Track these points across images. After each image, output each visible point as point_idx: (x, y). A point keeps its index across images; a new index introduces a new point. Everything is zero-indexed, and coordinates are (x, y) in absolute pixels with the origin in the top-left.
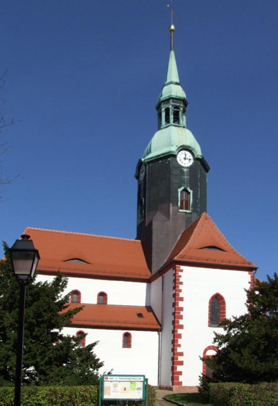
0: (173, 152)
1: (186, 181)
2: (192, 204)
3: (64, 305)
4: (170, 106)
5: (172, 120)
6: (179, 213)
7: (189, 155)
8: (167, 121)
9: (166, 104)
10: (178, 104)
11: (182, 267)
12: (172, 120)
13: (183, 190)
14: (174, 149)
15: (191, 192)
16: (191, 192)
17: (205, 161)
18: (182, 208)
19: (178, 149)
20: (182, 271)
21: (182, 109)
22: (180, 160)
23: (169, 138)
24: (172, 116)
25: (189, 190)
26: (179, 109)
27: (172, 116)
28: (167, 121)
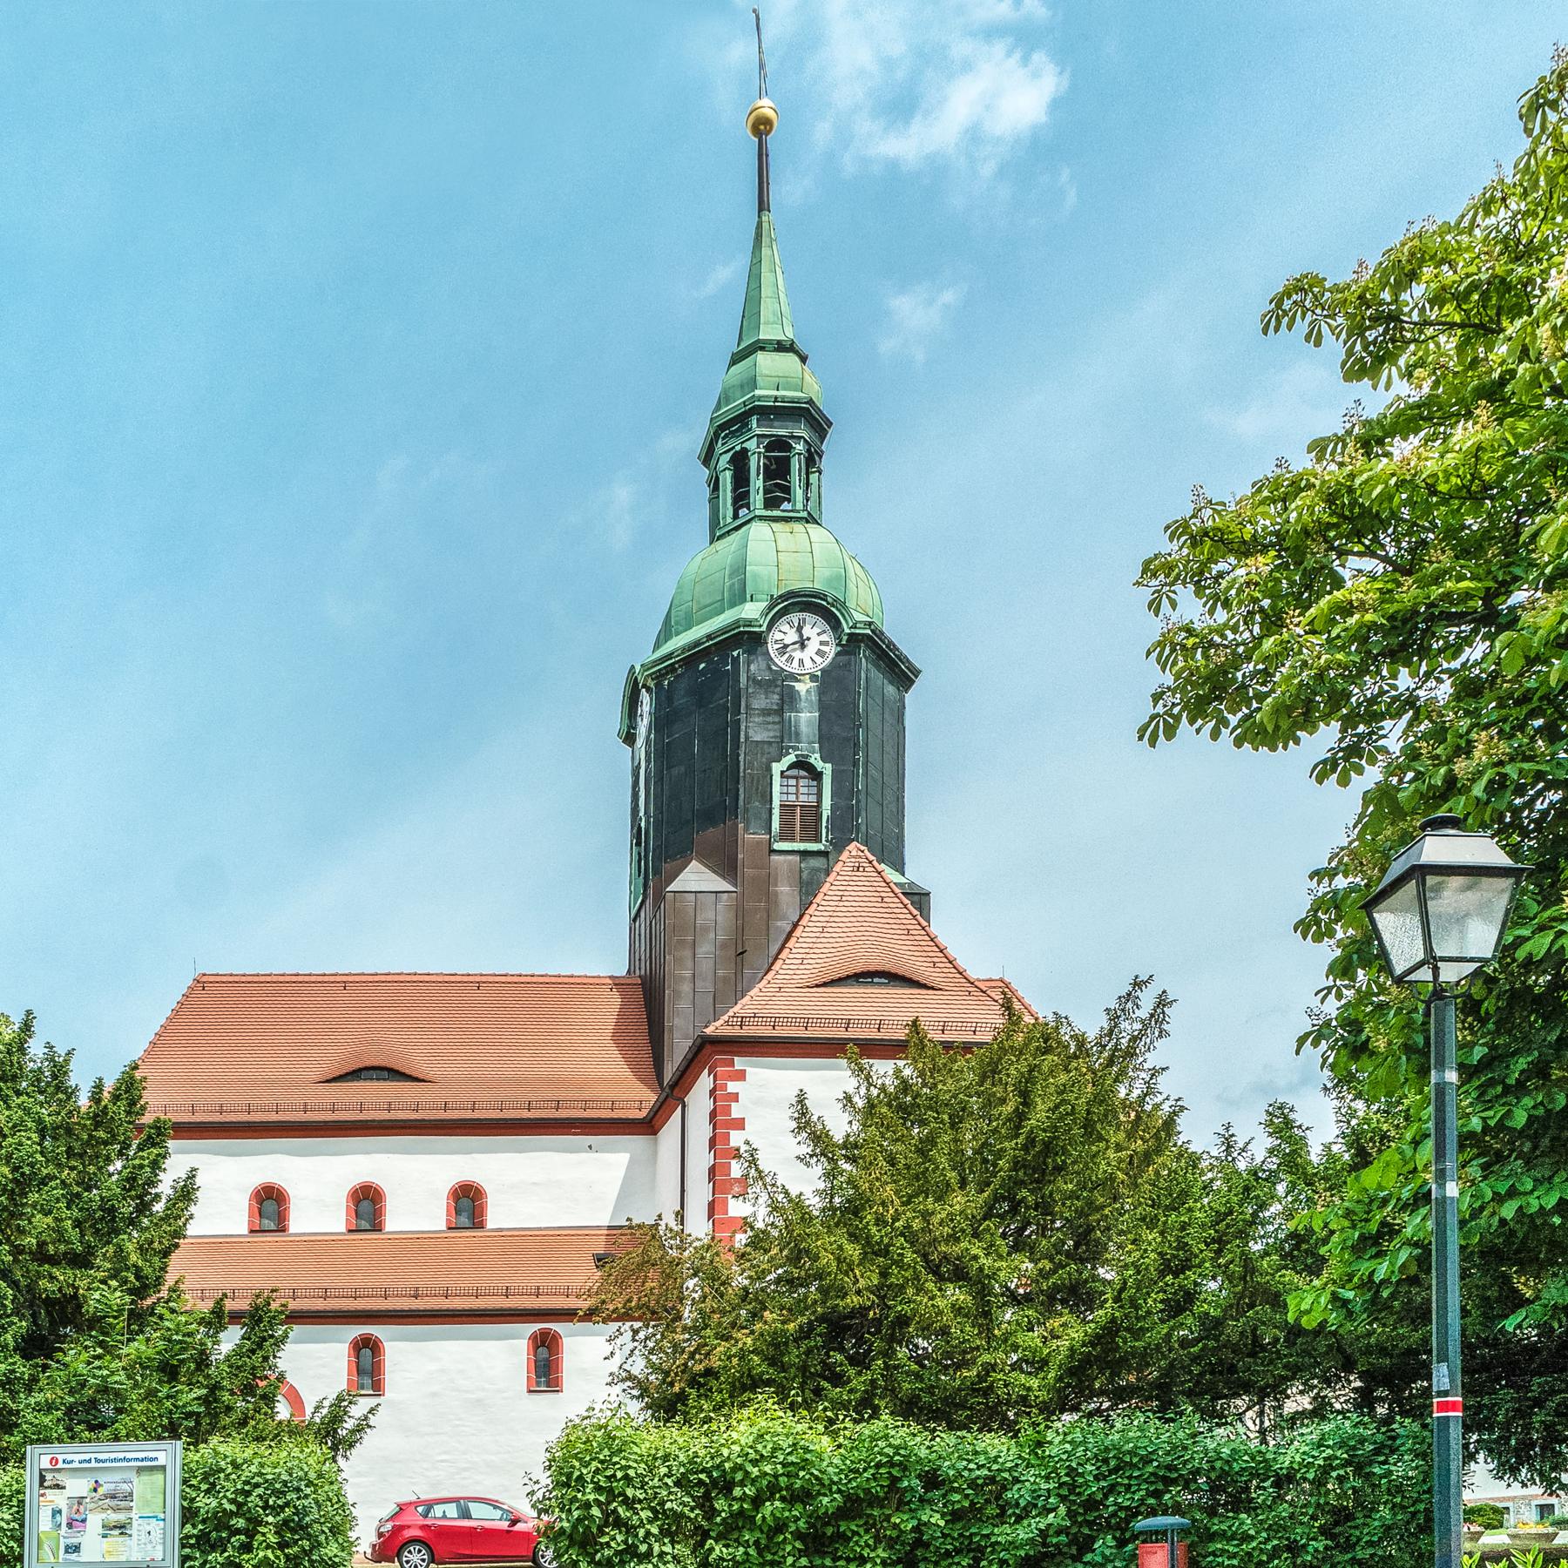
0: (749, 623)
1: (804, 729)
2: (831, 819)
3: (350, 1424)
4: (752, 445)
5: (757, 499)
6: (775, 858)
7: (816, 631)
8: (741, 499)
9: (733, 434)
10: (782, 432)
11: (739, 1063)
12: (757, 499)
13: (792, 767)
14: (752, 611)
15: (827, 769)
16: (827, 769)
17: (890, 644)
18: (786, 835)
19: (770, 608)
20: (741, 1076)
21: (800, 447)
22: (820, 653)
23: (740, 569)
24: (757, 483)
25: (819, 765)
26: (789, 448)
27: (757, 483)
28: (741, 499)
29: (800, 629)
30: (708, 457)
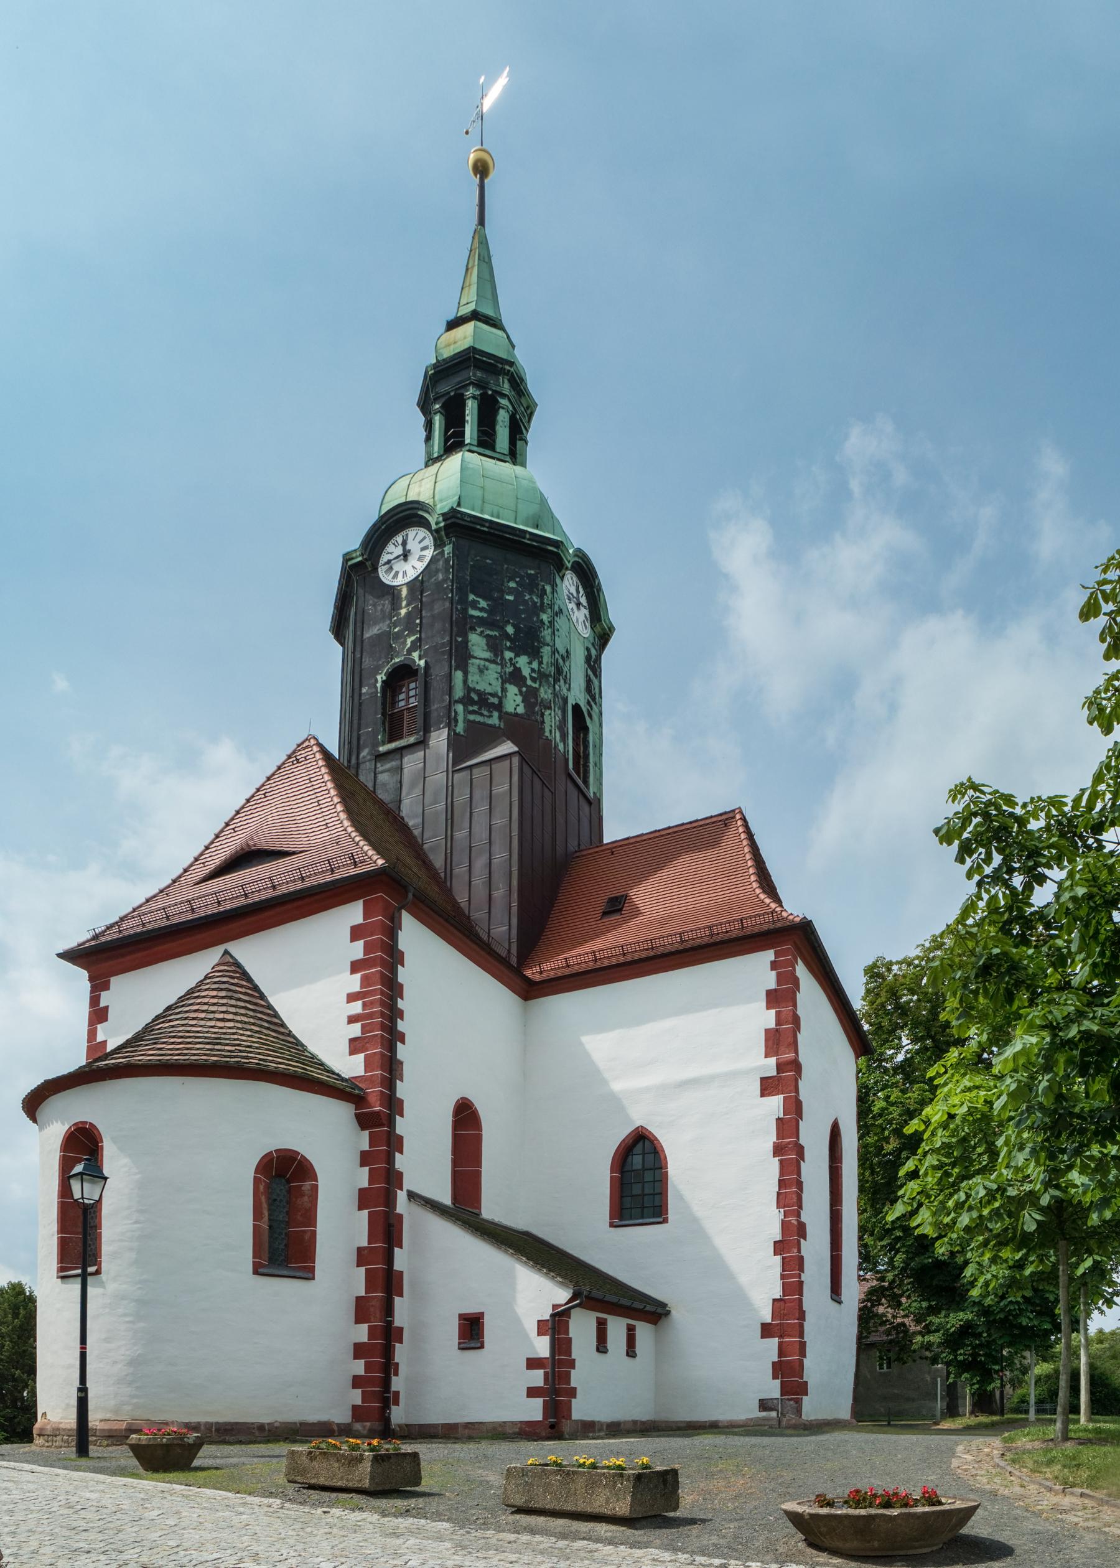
5: (470, 432)
12: (470, 432)
29: (404, 543)
30: (424, 405)
